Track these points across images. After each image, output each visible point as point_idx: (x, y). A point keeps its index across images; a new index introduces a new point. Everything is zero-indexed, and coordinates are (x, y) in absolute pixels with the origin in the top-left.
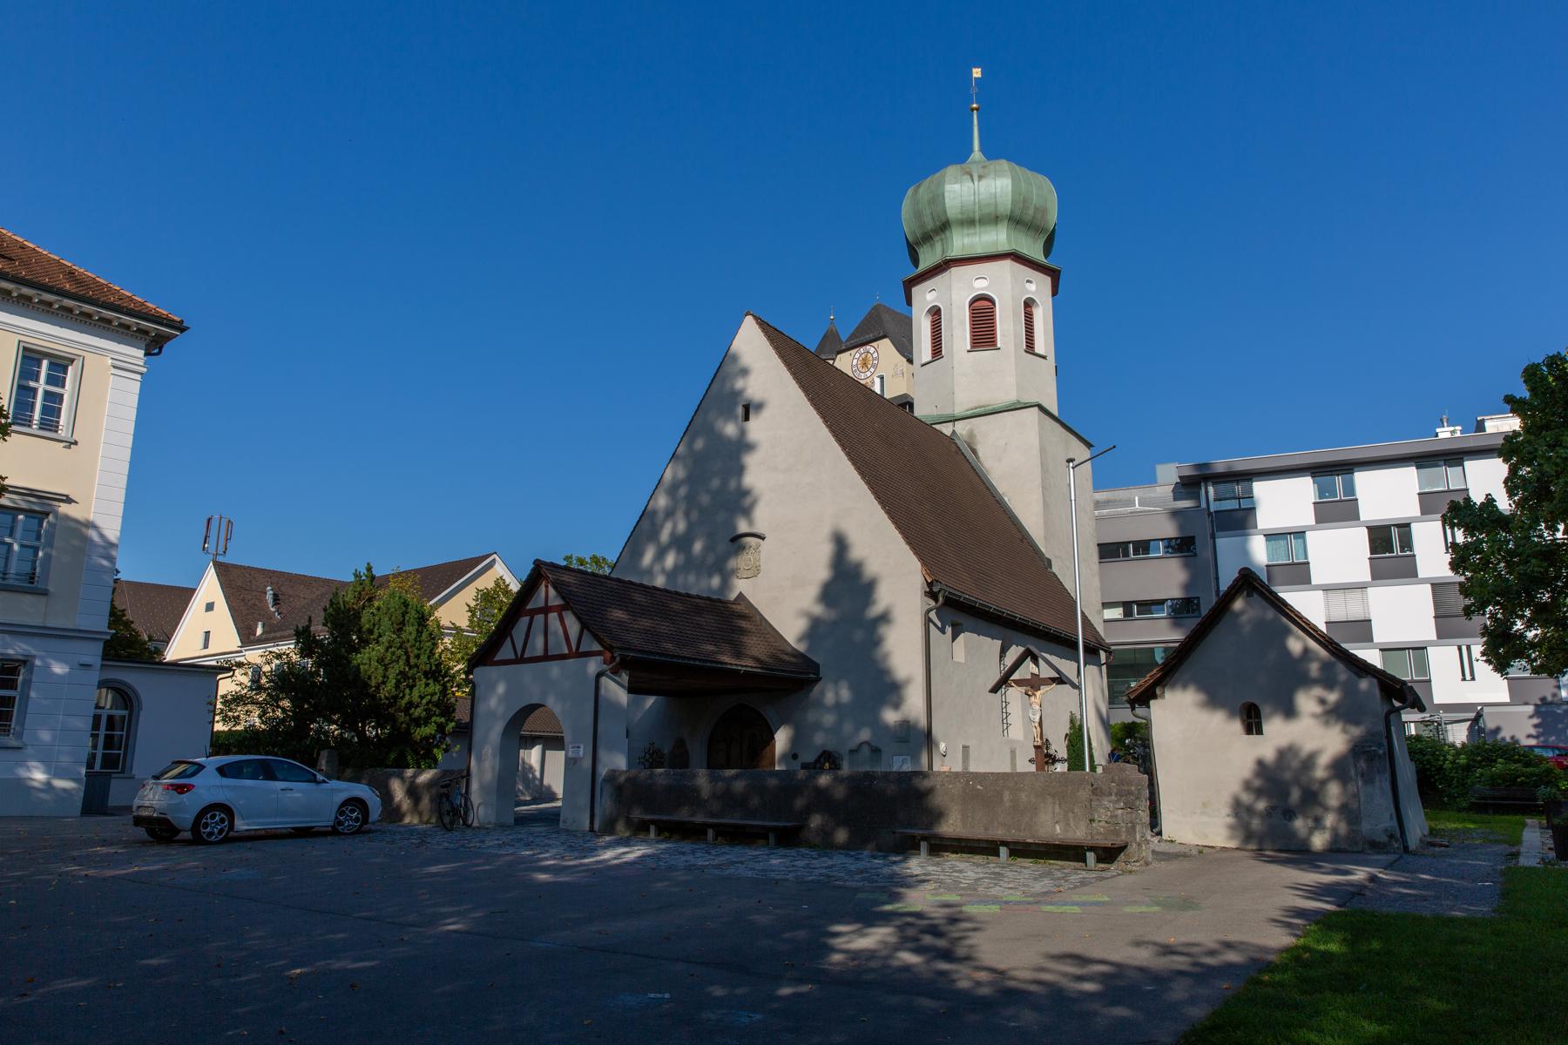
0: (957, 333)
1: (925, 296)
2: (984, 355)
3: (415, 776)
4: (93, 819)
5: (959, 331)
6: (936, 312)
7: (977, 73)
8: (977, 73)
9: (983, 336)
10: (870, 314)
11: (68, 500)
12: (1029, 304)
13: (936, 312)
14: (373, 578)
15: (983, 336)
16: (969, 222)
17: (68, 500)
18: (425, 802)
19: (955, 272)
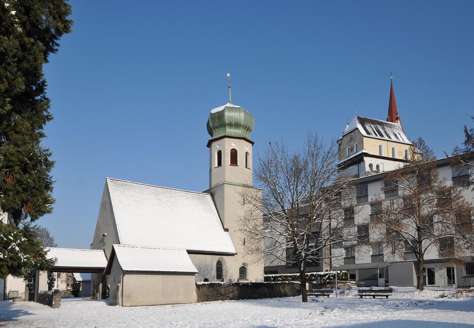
0: (226, 157)
1: (216, 146)
2: (234, 167)
3: (16, 23)
4: (120, 241)
5: (227, 158)
6: (220, 153)
7: (228, 75)
8: (228, 75)
9: (234, 161)
10: (217, 264)
11: (26, 313)
12: (247, 153)
13: (220, 153)
14: (17, 182)
15: (234, 161)
16: (231, 125)
17: (26, 313)
18: (35, 21)
19: (226, 139)
